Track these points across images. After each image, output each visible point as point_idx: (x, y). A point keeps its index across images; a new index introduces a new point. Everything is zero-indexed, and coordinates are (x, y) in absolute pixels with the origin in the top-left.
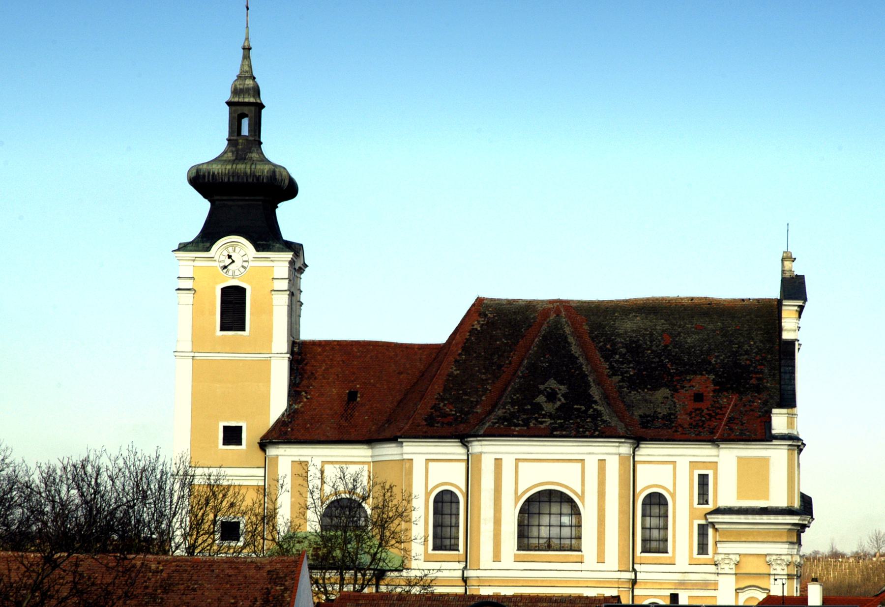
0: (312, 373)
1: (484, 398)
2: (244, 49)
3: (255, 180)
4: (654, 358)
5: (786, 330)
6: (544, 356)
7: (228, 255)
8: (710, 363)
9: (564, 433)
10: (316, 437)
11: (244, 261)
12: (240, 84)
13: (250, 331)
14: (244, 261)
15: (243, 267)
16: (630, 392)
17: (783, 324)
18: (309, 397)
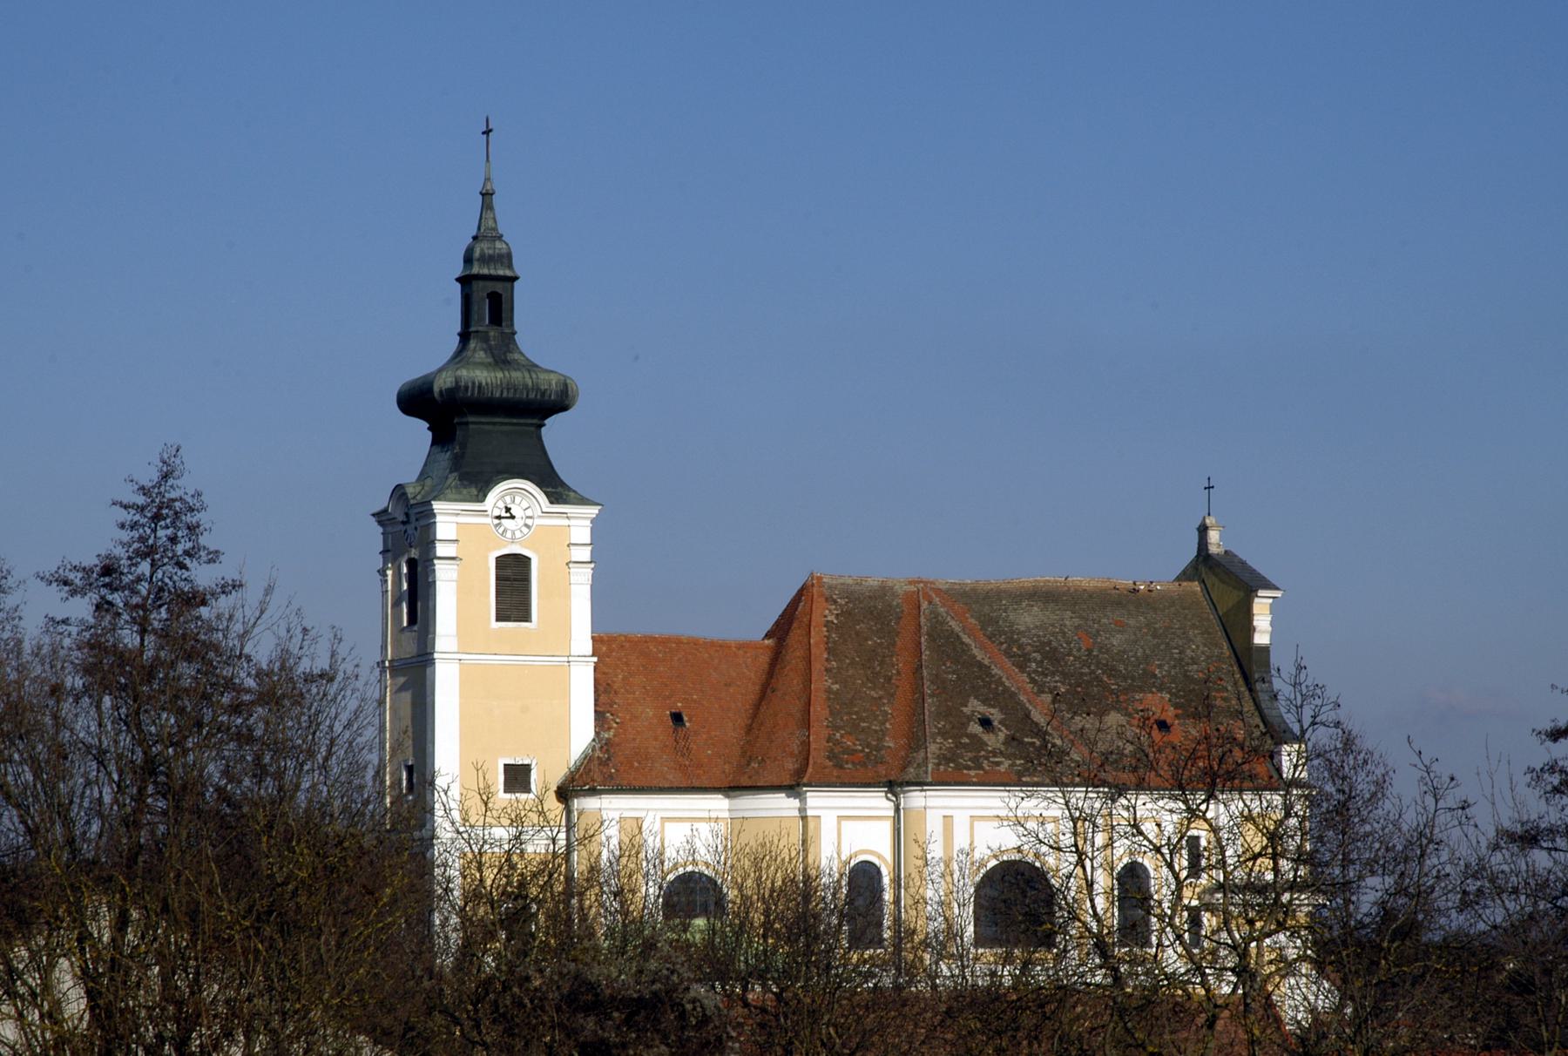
0: (608, 684)
1: (888, 726)
2: (483, 195)
3: (539, 397)
4: (1081, 668)
5: (1259, 632)
7: (506, 508)
8: (1155, 676)
9: (1035, 779)
10: (655, 783)
11: (528, 517)
12: (488, 248)
13: (538, 622)
14: (528, 517)
16: (1072, 718)
17: (1255, 623)
18: (618, 720)
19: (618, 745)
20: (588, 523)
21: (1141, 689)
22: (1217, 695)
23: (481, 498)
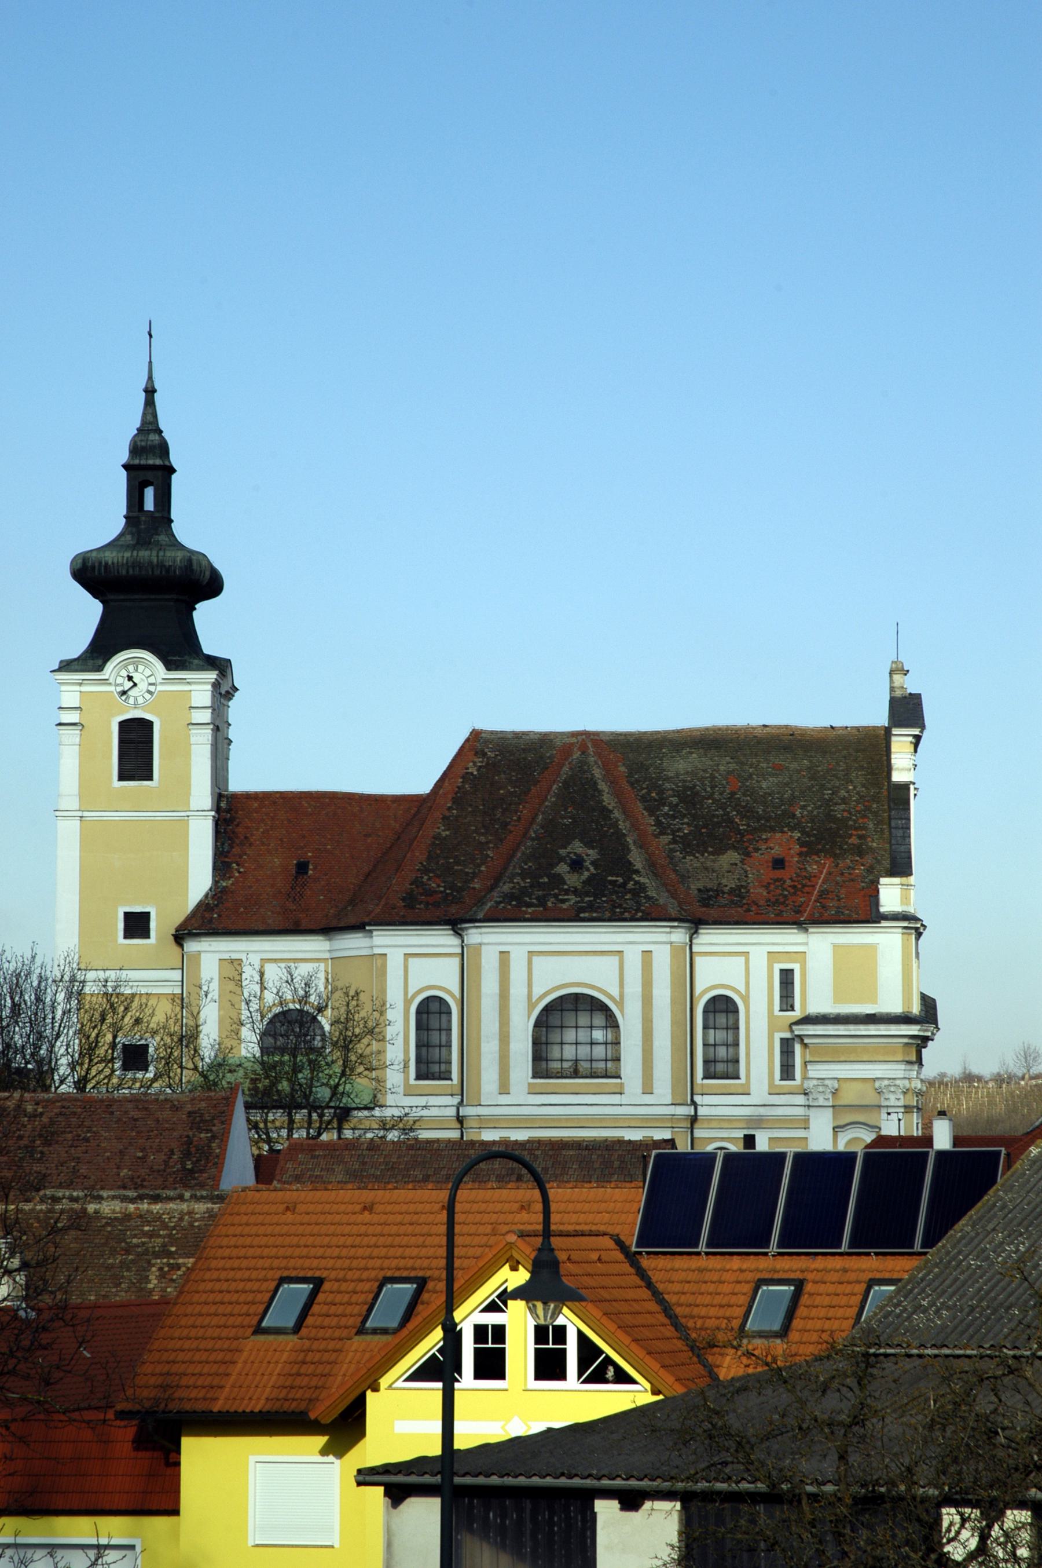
0: (246, 838)
1: (483, 868)
3: (164, 573)
7: (128, 676)
9: (594, 915)
12: (141, 441)
19: (232, 892)
20: (209, 687)
21: (772, 830)
22: (855, 833)
23: (100, 669)
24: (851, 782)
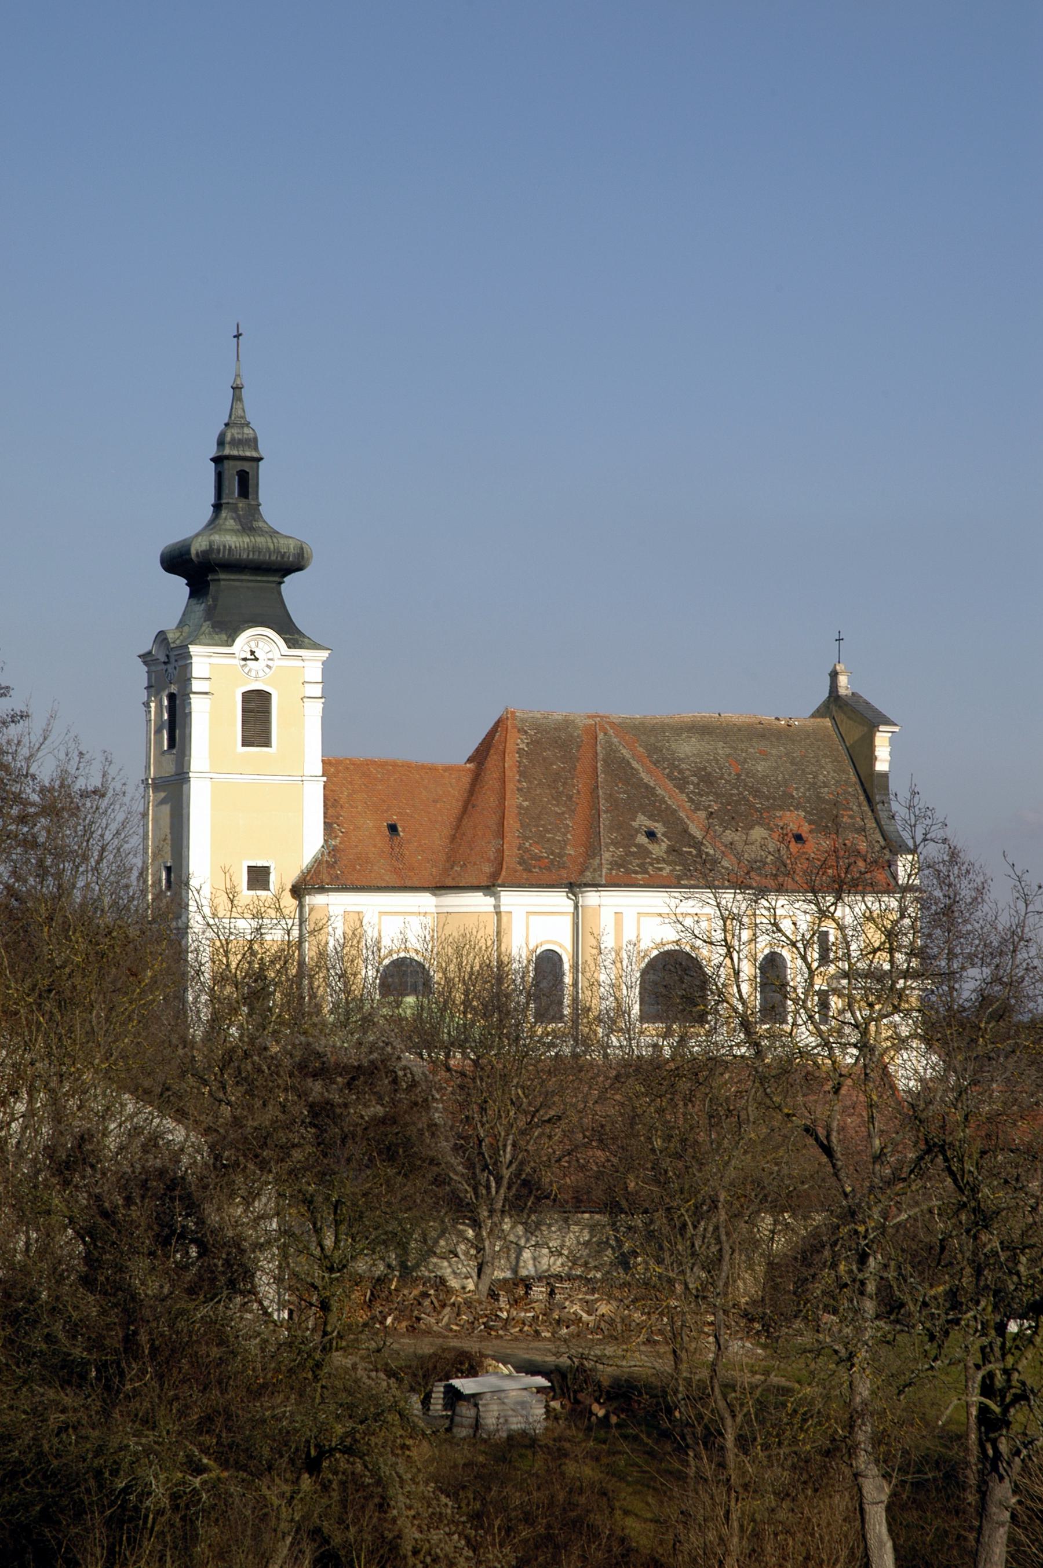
6: (617, 786)
15: (268, 666)
17: (877, 753)
24: (823, 767)
